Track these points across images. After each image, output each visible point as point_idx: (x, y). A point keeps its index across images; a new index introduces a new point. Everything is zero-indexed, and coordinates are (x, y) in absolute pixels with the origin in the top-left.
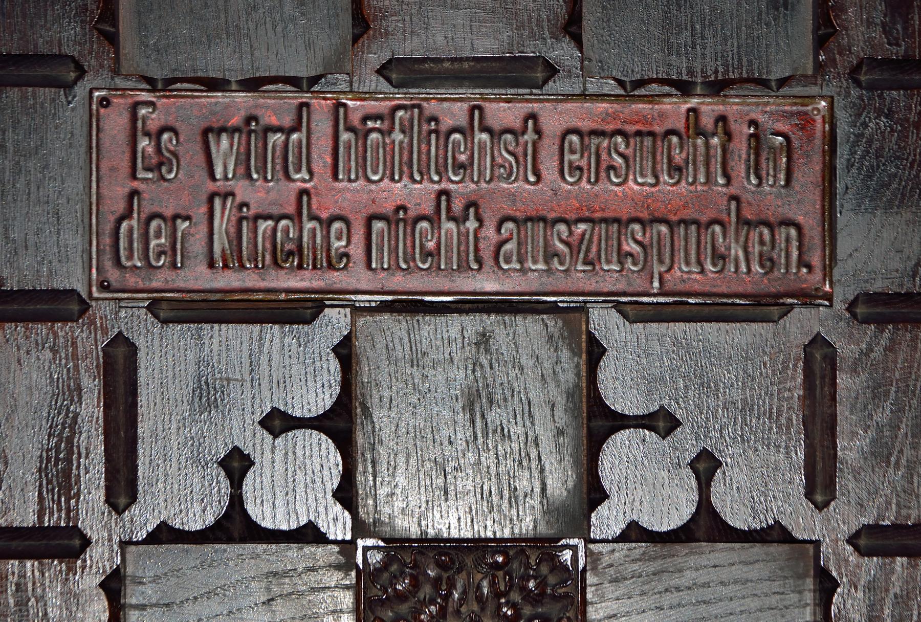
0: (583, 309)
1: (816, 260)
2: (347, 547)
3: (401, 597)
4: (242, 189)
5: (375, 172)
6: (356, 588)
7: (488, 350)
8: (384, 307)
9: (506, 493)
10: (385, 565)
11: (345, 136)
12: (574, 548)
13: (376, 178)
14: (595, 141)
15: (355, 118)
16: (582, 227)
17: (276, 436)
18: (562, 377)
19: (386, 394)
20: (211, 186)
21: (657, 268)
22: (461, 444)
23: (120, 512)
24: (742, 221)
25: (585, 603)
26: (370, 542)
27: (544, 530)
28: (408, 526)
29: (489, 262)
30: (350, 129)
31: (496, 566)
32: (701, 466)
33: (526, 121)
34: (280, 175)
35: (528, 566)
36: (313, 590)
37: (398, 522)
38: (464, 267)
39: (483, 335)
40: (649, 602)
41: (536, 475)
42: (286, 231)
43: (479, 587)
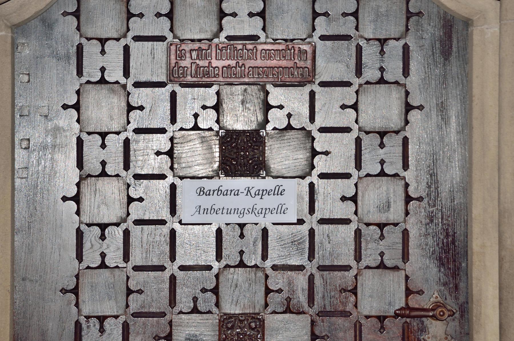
0: (265, 84)
1: (311, 75)
2: (218, 132)
3: (228, 142)
4: (197, 61)
5: (224, 58)
6: (219, 140)
7: (246, 92)
8: (225, 84)
9: (250, 121)
10: (226, 135)
11: (218, 51)
12: (263, 132)
13: (224, 59)
14: (268, 52)
15: (220, 48)
16: (265, 68)
17: (204, 110)
18: (261, 97)
19: (226, 101)
20: (192, 61)
21: (280, 77)
22: (240, 111)
23: (173, 125)
24: (297, 67)
25: (265, 143)
26: (223, 131)
27: (257, 128)
28: (230, 127)
29: (246, 76)
30: (219, 49)
31: (247, 135)
32: (289, 116)
33: (254, 47)
34: (205, 59)
35: (254, 136)
36: (211, 140)
37: (228, 127)
38: (241, 77)
39: (245, 89)
40: (279, 142)
41: (256, 117)
42: (206, 70)
43: (244, 140)
